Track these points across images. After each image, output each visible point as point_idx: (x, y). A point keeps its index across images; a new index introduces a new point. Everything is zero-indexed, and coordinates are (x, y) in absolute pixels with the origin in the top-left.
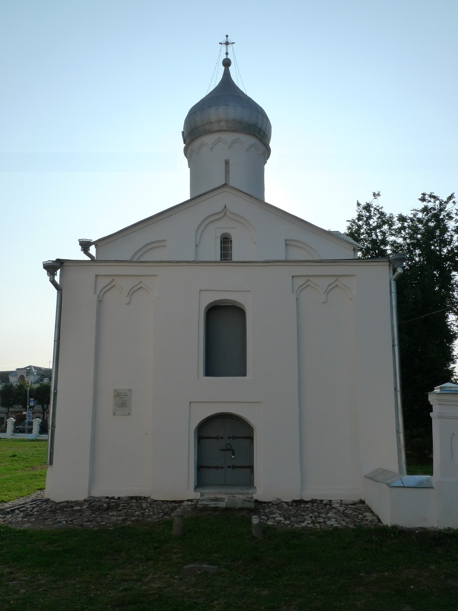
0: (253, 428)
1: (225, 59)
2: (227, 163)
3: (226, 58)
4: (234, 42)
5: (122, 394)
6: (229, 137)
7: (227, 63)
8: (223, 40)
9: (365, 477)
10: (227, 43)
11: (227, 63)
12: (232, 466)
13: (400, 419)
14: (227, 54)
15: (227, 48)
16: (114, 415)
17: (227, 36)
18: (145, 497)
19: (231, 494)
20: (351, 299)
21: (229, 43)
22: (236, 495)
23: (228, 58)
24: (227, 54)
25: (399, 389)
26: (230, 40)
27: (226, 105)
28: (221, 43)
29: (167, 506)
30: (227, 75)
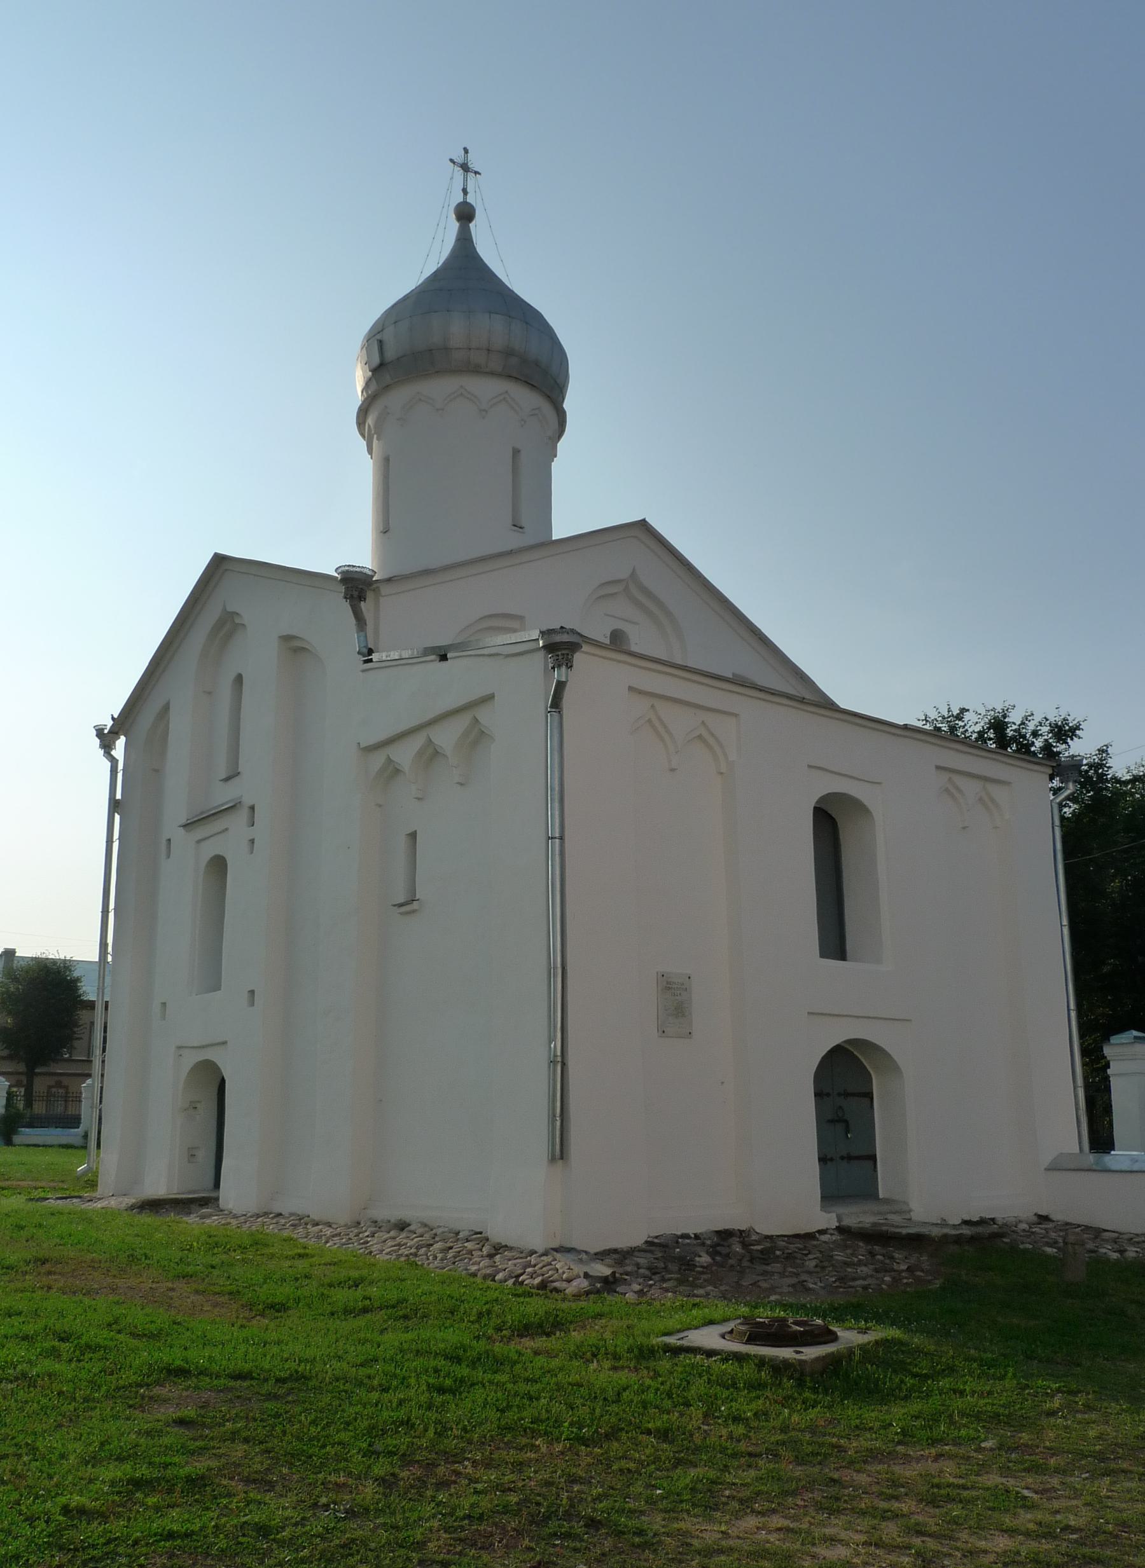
0: (871, 1075)
1: (461, 202)
2: (516, 452)
3: (462, 200)
4: (480, 172)
5: (676, 986)
6: (486, 388)
7: (465, 214)
8: (459, 157)
9: (1045, 1169)
10: (465, 168)
11: (465, 214)
12: (846, 1156)
13: (99, 1015)
14: (465, 192)
15: (465, 180)
16: (664, 1035)
17: (466, 151)
18: (741, 1232)
19: (879, 1213)
20: (996, 828)
21: (469, 168)
22: (889, 1217)
23: (468, 201)
24: (465, 192)
25: (1072, 1006)
26: (474, 164)
27: (490, 313)
28: (452, 161)
29: (271, 1244)
30: (465, 244)
